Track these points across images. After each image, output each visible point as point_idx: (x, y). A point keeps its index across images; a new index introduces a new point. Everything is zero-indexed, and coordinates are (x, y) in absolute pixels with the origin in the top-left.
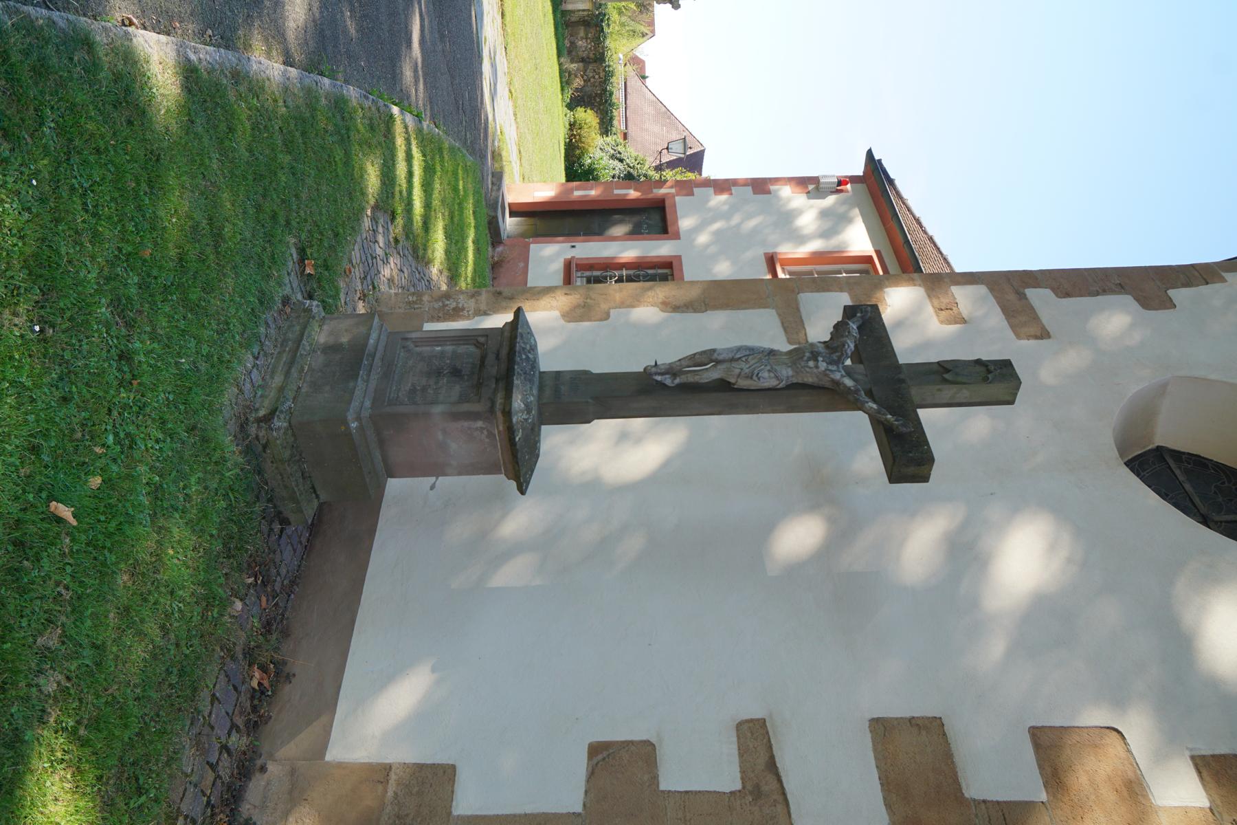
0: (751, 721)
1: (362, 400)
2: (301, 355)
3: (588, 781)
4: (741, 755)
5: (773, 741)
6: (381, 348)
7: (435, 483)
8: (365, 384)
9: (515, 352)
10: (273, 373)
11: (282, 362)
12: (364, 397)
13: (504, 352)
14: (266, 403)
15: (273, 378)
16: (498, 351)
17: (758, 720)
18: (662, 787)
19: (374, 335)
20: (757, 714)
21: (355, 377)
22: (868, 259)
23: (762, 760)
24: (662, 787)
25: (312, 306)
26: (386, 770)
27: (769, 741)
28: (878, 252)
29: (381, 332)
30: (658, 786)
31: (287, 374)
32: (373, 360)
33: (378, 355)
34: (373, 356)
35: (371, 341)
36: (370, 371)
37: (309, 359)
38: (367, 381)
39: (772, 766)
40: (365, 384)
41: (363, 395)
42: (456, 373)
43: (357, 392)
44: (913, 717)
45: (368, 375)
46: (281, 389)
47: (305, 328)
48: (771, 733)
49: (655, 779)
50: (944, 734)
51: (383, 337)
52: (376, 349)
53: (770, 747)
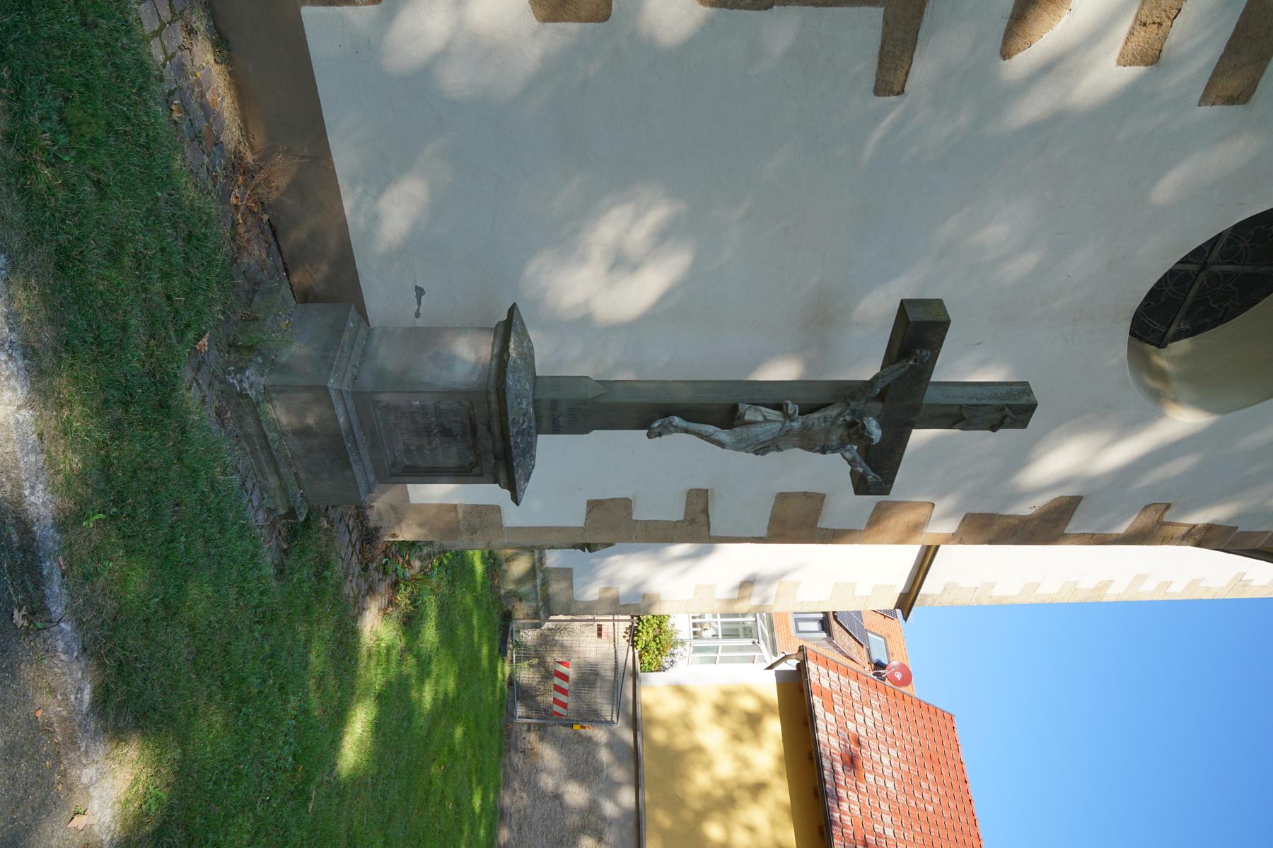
0: (699, 490)
1: (365, 479)
2: (277, 450)
3: (587, 514)
4: (687, 506)
5: (710, 501)
6: (354, 417)
7: (418, 310)
8: (360, 463)
9: (511, 447)
10: (263, 475)
11: (264, 463)
12: (366, 476)
13: (496, 429)
14: (278, 502)
15: (267, 479)
16: (489, 422)
17: (703, 490)
18: (634, 518)
19: (340, 411)
20: (703, 485)
21: (348, 465)
23: (701, 506)
24: (634, 518)
25: (246, 390)
26: (454, 507)
27: (707, 500)
29: (343, 400)
30: (631, 517)
31: (277, 472)
32: (354, 436)
33: (355, 427)
34: (351, 431)
35: (342, 420)
36: (358, 450)
37: (285, 443)
38: (360, 460)
39: (705, 511)
40: (360, 463)
41: (364, 474)
42: (446, 432)
43: (358, 478)
44: (807, 492)
45: (358, 454)
46: (284, 489)
47: (258, 421)
48: (709, 498)
49: (630, 514)
50: (823, 501)
51: (350, 405)
52: (351, 426)
53: (707, 503)
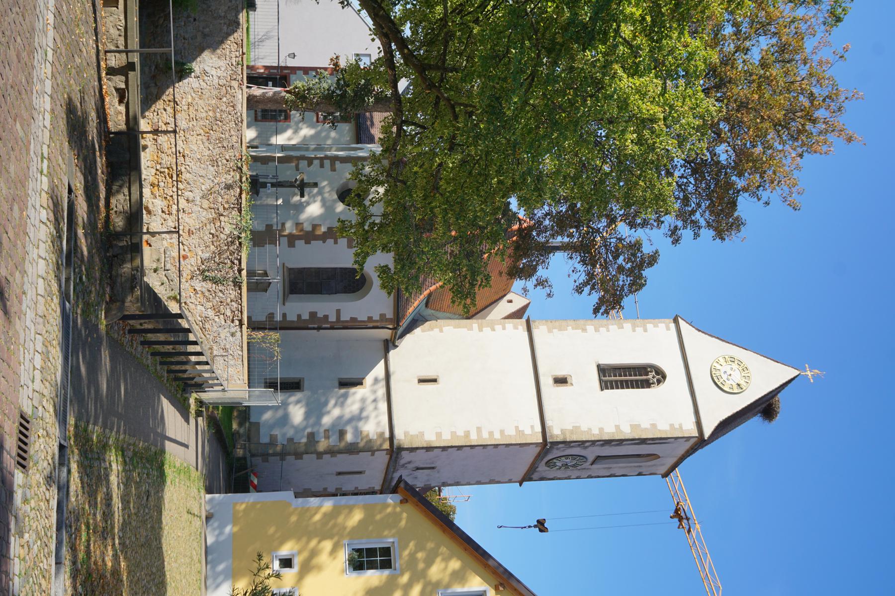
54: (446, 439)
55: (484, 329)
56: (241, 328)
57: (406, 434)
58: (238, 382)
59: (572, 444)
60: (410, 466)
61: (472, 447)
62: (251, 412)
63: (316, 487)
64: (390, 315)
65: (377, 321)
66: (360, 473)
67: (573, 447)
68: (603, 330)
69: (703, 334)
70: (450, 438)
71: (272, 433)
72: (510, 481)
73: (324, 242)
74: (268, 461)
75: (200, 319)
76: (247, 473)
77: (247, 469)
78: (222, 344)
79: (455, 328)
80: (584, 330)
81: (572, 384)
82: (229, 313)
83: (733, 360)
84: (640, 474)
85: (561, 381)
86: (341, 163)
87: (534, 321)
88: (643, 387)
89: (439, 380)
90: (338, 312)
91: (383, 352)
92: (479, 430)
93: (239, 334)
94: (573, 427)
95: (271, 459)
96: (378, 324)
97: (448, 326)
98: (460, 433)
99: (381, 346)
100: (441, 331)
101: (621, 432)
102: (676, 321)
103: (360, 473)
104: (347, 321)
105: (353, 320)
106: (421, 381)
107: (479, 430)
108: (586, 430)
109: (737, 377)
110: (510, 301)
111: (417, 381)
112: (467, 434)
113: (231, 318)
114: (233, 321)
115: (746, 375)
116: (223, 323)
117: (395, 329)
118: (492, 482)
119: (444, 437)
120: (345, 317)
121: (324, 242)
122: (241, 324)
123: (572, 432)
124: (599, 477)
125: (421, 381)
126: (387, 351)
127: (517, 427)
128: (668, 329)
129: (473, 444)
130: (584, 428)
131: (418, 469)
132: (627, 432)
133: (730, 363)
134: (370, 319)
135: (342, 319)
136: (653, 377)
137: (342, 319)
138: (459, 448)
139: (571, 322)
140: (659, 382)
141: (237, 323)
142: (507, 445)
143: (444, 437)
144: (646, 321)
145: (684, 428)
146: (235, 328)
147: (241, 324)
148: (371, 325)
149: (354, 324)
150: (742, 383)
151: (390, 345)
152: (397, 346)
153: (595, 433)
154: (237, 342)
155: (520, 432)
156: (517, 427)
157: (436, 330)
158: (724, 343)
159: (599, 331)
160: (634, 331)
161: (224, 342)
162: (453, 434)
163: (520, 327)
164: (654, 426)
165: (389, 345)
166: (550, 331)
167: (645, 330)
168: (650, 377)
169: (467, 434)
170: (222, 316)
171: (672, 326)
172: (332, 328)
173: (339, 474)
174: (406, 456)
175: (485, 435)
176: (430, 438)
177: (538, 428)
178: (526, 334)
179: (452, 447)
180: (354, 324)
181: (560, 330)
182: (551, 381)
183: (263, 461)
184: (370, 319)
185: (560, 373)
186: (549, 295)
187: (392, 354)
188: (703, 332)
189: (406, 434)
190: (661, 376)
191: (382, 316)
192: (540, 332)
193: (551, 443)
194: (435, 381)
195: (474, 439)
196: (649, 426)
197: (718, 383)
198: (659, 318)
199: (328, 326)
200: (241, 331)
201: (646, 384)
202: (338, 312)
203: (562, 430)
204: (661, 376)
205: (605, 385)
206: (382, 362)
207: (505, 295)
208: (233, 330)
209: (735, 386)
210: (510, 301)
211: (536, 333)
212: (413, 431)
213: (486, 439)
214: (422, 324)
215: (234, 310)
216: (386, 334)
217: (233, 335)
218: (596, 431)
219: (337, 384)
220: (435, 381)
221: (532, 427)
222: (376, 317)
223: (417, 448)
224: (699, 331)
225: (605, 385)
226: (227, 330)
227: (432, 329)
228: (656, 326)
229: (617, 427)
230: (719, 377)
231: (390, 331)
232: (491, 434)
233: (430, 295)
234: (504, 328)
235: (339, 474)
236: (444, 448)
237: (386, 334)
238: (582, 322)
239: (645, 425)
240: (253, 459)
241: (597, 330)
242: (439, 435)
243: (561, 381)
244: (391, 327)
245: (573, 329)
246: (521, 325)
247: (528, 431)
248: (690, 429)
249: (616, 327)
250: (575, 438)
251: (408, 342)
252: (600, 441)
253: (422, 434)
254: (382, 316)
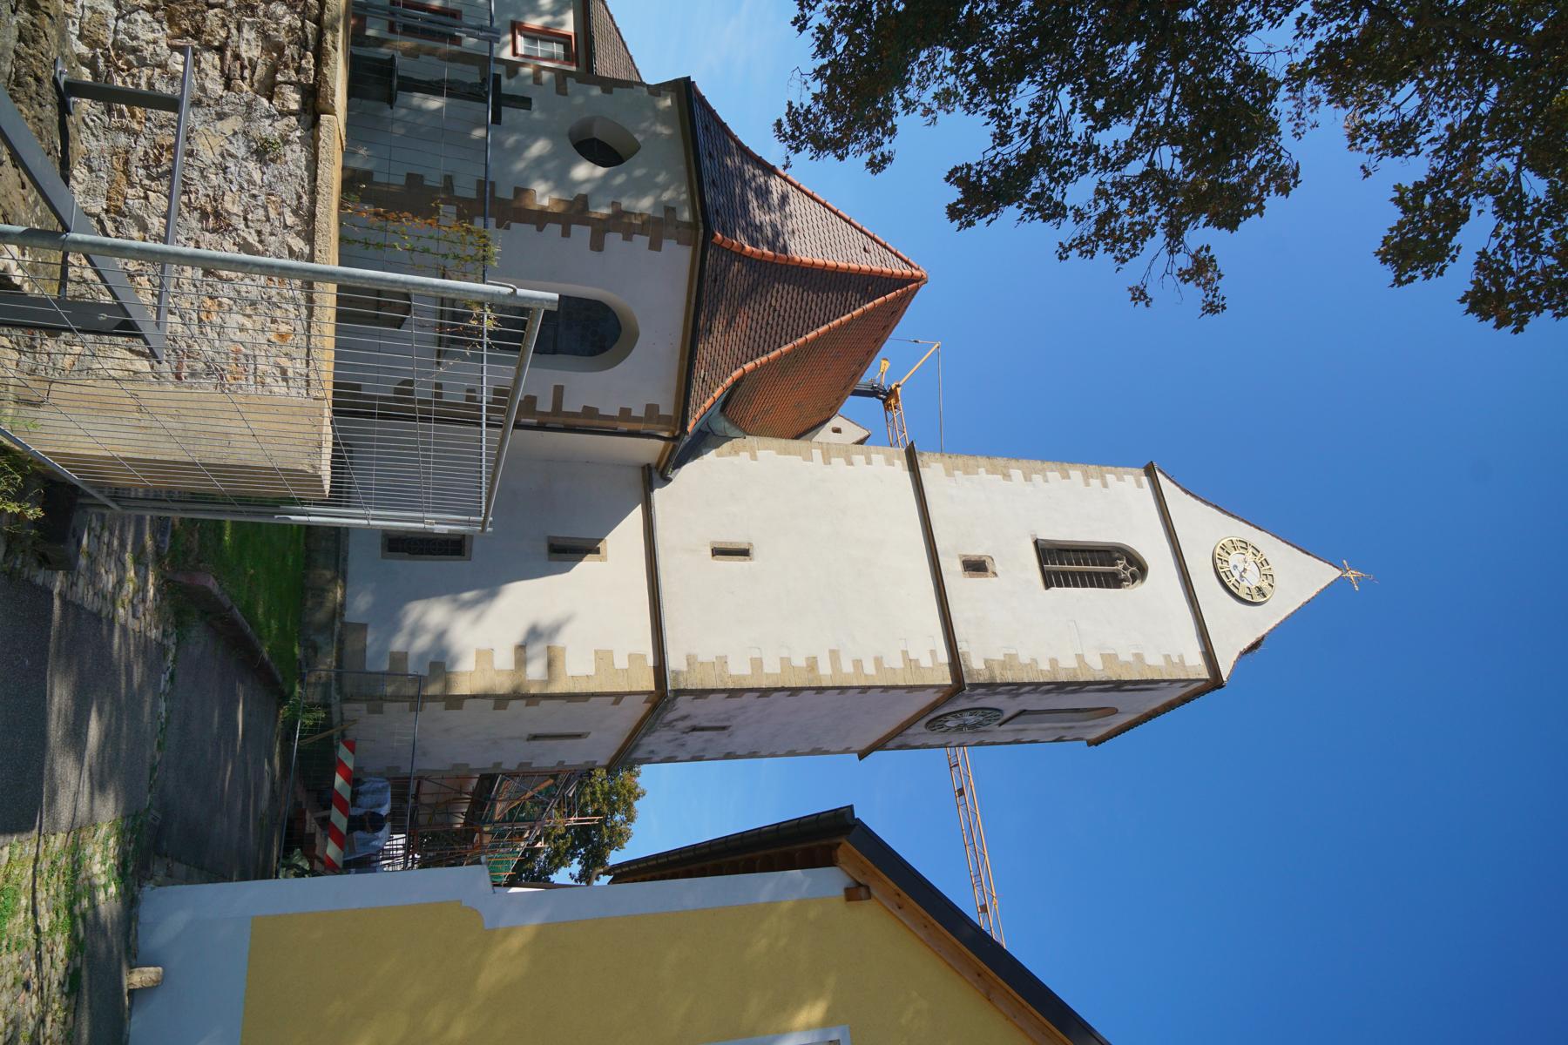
22: (569, 37)
28: (575, 34)
54: (772, 673)
55: (833, 460)
56: (314, 124)
57: (691, 660)
58: (280, 389)
59: (1000, 689)
60: (682, 725)
61: (820, 690)
62: (352, 539)
63: (104, 330)
64: (667, 408)
65: (638, 420)
66: (578, 736)
67: (999, 693)
68: (1037, 478)
69: (1193, 499)
70: (778, 671)
71: (370, 630)
72: (847, 751)
73: (540, 229)
74: (381, 712)
75: (82, 49)
76: (331, 738)
77: (332, 728)
78: (199, 185)
79: (779, 453)
80: (1007, 476)
81: (995, 574)
82: (250, 47)
83: (1244, 545)
84: (1059, 740)
85: (976, 567)
86: (578, 81)
87: (921, 454)
88: (1108, 586)
89: (755, 552)
90: (559, 391)
91: (640, 491)
92: (834, 655)
93: (295, 155)
94: (1005, 655)
95: (387, 706)
96: (641, 427)
97: (766, 448)
98: (799, 661)
99: (636, 477)
100: (754, 457)
101: (1088, 667)
102: (1150, 471)
103: (578, 736)
104: (575, 415)
105: (590, 412)
106: (719, 552)
107: (834, 655)
108: (1028, 661)
109: (1253, 579)
110: (837, 431)
111: (710, 553)
112: (812, 664)
113: (261, 71)
114: (269, 89)
115: (1267, 572)
116: (215, 87)
117: (674, 438)
118: (816, 751)
119: (767, 669)
120: (572, 405)
121: (540, 229)
122: (313, 105)
123: (1004, 665)
124: (994, 744)
125: (719, 552)
126: (648, 488)
127: (905, 653)
128: (1140, 485)
129: (824, 684)
130: (1024, 658)
131: (694, 729)
132: (1096, 668)
133: (1242, 551)
134: (625, 413)
135: (566, 408)
136: (1125, 568)
137: (566, 408)
138: (794, 691)
139: (982, 461)
140: (1134, 578)
141: (293, 100)
142: (886, 688)
143: (767, 669)
144: (1104, 468)
145: (1188, 663)
146: (281, 125)
147: (313, 105)
148: (624, 427)
149: (589, 423)
150: (1264, 585)
151: (656, 476)
152: (669, 480)
153: (1043, 671)
154: (287, 191)
155: (911, 663)
156: (905, 653)
157: (745, 455)
158: (1225, 516)
159: (1031, 481)
160: (1087, 484)
161: (215, 180)
162: (785, 661)
163: (897, 462)
164: (1139, 657)
165: (654, 475)
166: (949, 474)
167: (1105, 485)
168: (1120, 567)
169: (812, 664)
170: (210, 60)
171: (1145, 480)
172: (541, 427)
173: (535, 737)
174: (683, 705)
175: (847, 667)
176: (739, 671)
177: (943, 656)
178: (906, 476)
179: (783, 689)
180: (589, 423)
181: (966, 473)
182: (959, 567)
183: (371, 711)
184: (625, 413)
185: (975, 552)
186: (1212, 308)
187: (658, 494)
188: (1193, 495)
189: (691, 660)
190: (1139, 570)
191: (652, 409)
192: (932, 471)
193: (970, 685)
194: (744, 553)
195: (826, 674)
196: (1131, 659)
197: (1230, 584)
198: (1123, 466)
199: (533, 421)
200: (312, 143)
201: (1113, 581)
202: (559, 391)
203: (986, 661)
204: (1139, 570)
205: (1050, 580)
206: (638, 512)
207: (828, 420)
208: (266, 129)
209: (1254, 592)
210: (837, 431)
211: (926, 474)
212: (705, 655)
213: (848, 674)
214: (717, 446)
215: (283, 37)
216: (650, 449)
217: (263, 152)
218: (1045, 666)
219: (544, 548)
220: (744, 553)
221: (933, 653)
222: (639, 411)
223: (713, 691)
224: (1187, 492)
225: (1050, 580)
226: (233, 124)
227: (737, 453)
228: (1120, 479)
229: (1080, 657)
230: (1228, 573)
231: (661, 443)
232: (858, 664)
233: (737, 384)
234: (869, 462)
235: (535, 737)
236: (765, 692)
237: (650, 449)
238: (1000, 462)
239: (1125, 656)
240: (347, 707)
241: (1027, 478)
242: (757, 663)
243: (976, 567)
244: (666, 434)
245: (988, 472)
246: (899, 459)
247: (926, 662)
248: (1195, 666)
249: (1057, 474)
250: (1009, 677)
251: (689, 475)
252: (1048, 684)
253: (723, 661)
254: (652, 409)
